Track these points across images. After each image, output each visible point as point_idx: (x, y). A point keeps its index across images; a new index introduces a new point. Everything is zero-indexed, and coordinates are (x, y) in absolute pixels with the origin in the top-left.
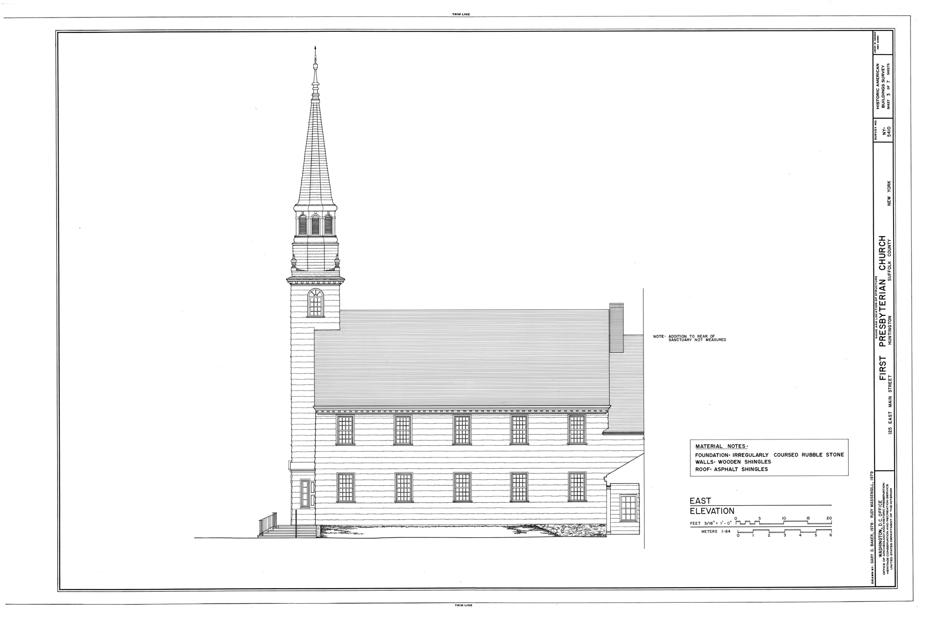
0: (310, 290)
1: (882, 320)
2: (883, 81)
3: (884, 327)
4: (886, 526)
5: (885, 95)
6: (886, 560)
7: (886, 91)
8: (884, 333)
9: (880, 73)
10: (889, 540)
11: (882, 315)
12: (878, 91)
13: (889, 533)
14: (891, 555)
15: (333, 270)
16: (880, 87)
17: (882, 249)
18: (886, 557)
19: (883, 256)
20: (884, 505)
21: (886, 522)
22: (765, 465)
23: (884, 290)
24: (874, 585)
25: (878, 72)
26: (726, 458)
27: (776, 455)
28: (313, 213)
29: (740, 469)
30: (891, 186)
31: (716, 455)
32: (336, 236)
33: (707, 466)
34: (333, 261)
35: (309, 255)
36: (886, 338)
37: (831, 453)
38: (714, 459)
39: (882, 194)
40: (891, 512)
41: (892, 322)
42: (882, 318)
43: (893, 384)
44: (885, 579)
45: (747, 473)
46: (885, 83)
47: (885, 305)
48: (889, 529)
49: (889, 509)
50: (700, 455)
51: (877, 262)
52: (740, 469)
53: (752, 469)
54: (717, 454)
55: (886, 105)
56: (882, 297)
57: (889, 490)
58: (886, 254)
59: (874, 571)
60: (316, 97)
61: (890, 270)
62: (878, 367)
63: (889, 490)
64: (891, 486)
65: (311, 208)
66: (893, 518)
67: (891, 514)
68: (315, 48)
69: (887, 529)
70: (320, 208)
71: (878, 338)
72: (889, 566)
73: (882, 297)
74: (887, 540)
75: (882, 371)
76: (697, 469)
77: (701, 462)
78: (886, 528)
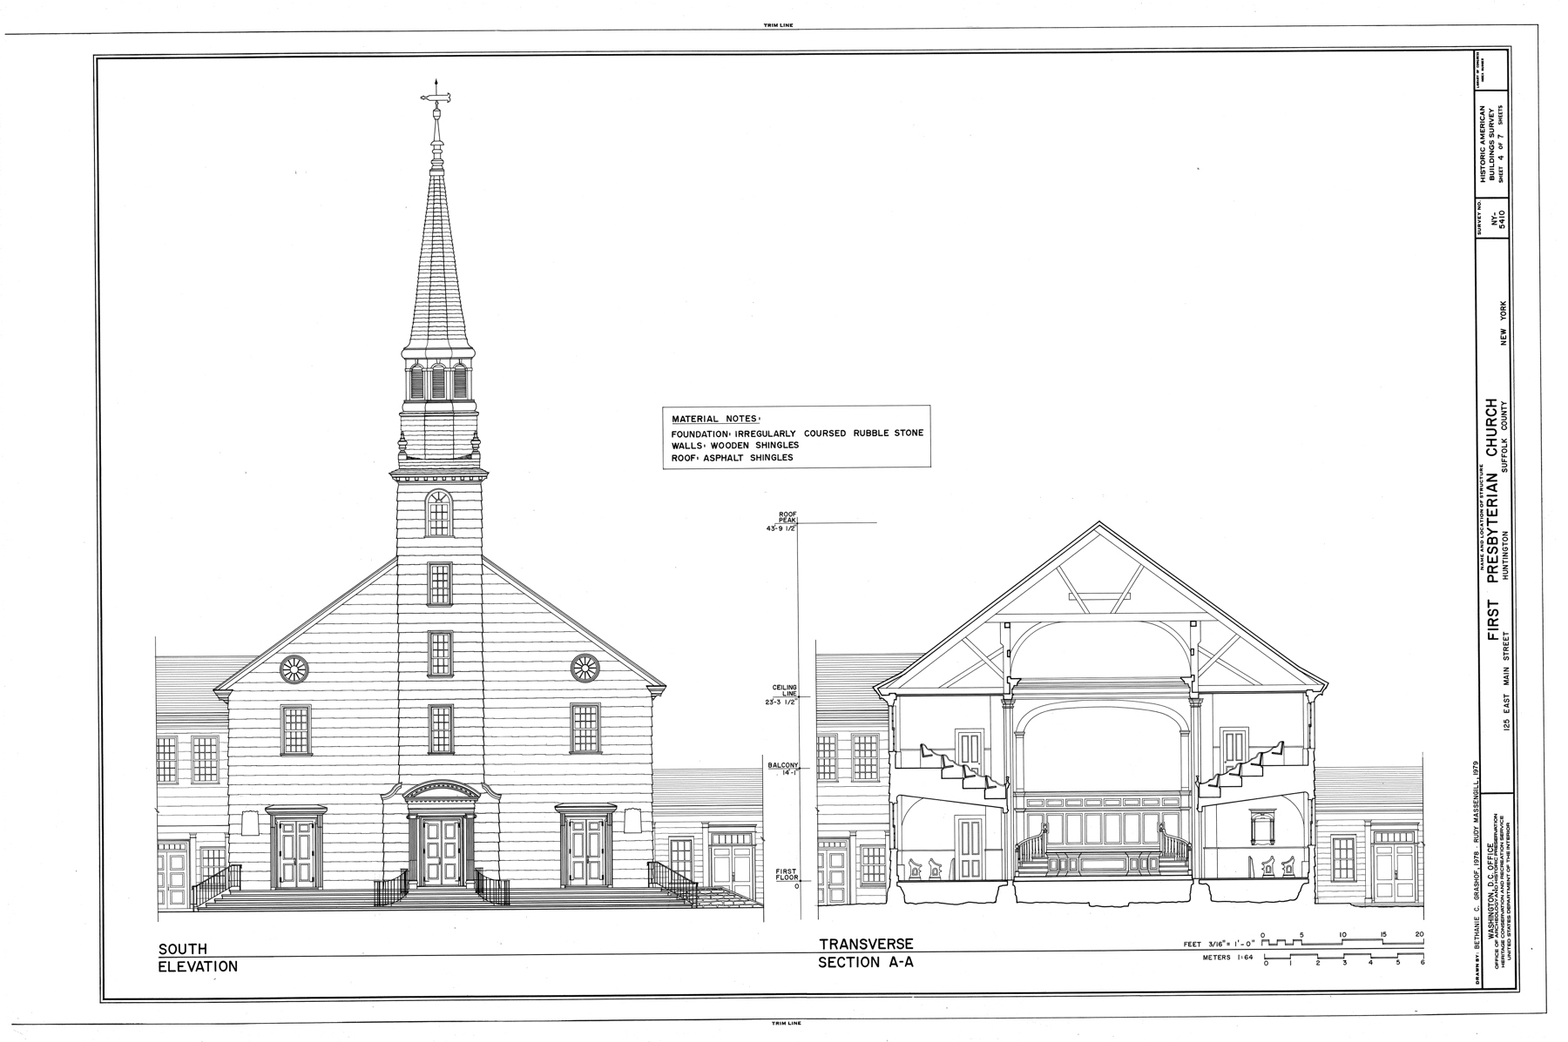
0: (429, 493)
1: (1492, 539)
2: (1492, 135)
3: (1495, 550)
4: (1500, 887)
5: (1496, 158)
6: (1500, 943)
7: (1497, 152)
8: (1495, 560)
9: (1487, 121)
10: (1505, 910)
11: (1492, 532)
12: (1483, 151)
13: (1506, 899)
14: (1509, 935)
15: (469, 457)
16: (1487, 145)
17: (1492, 421)
18: (1499, 940)
19: (1493, 432)
20: (1496, 852)
21: (1499, 880)
22: (788, 451)
23: (1494, 490)
24: (1479, 986)
25: (1482, 121)
26: (724, 440)
27: (807, 433)
28: (435, 361)
29: (746, 458)
30: (1506, 309)
31: (707, 434)
32: (473, 401)
33: (690, 452)
34: (469, 442)
35: (427, 442)
36: (1500, 569)
37: (903, 431)
38: (702, 440)
39: (1492, 324)
40: (1508, 863)
41: (1509, 542)
42: (1492, 535)
43: (1510, 648)
44: (1493, 978)
45: (758, 463)
46: (1495, 138)
47: (1496, 515)
48: (1505, 891)
49: (1505, 857)
50: (680, 434)
51: (1483, 443)
52: (746, 458)
53: (767, 457)
54: (688, 417)
55: (1497, 176)
56: (1491, 503)
57: (1505, 825)
58: (1498, 428)
59: (1480, 963)
60: (437, 166)
61: (1506, 455)
62: (1485, 618)
63: (1505, 825)
64: (1509, 819)
65: (430, 354)
66: (1512, 873)
67: (1508, 867)
68: (436, 83)
69: (1502, 891)
70: (448, 353)
71: (1485, 569)
72: (1506, 953)
73: (1492, 502)
74: (1502, 910)
75: (1493, 625)
76: (674, 458)
77: (682, 446)
78: (1499, 890)
